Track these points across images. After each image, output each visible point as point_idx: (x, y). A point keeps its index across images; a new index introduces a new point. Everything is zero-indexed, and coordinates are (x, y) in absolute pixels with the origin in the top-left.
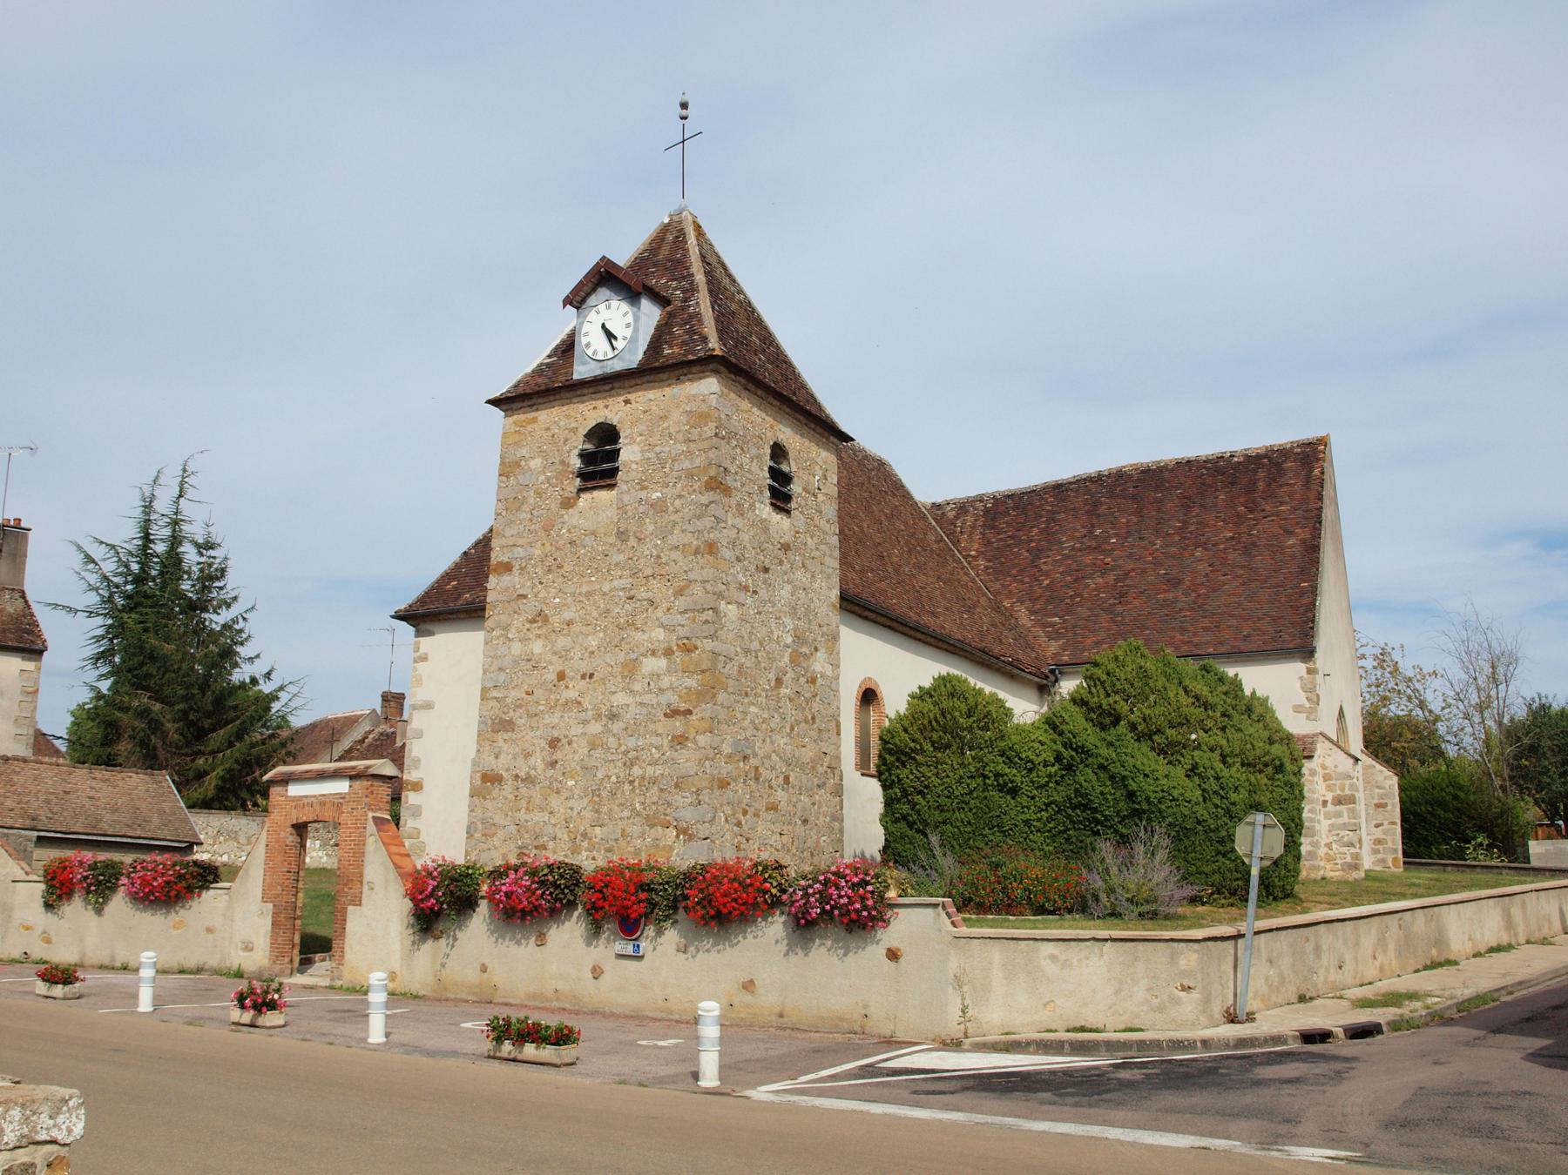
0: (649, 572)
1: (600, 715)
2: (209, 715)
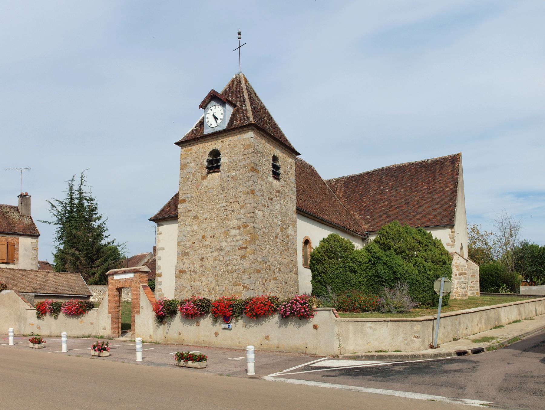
0: (232, 201)
2: (95, 255)
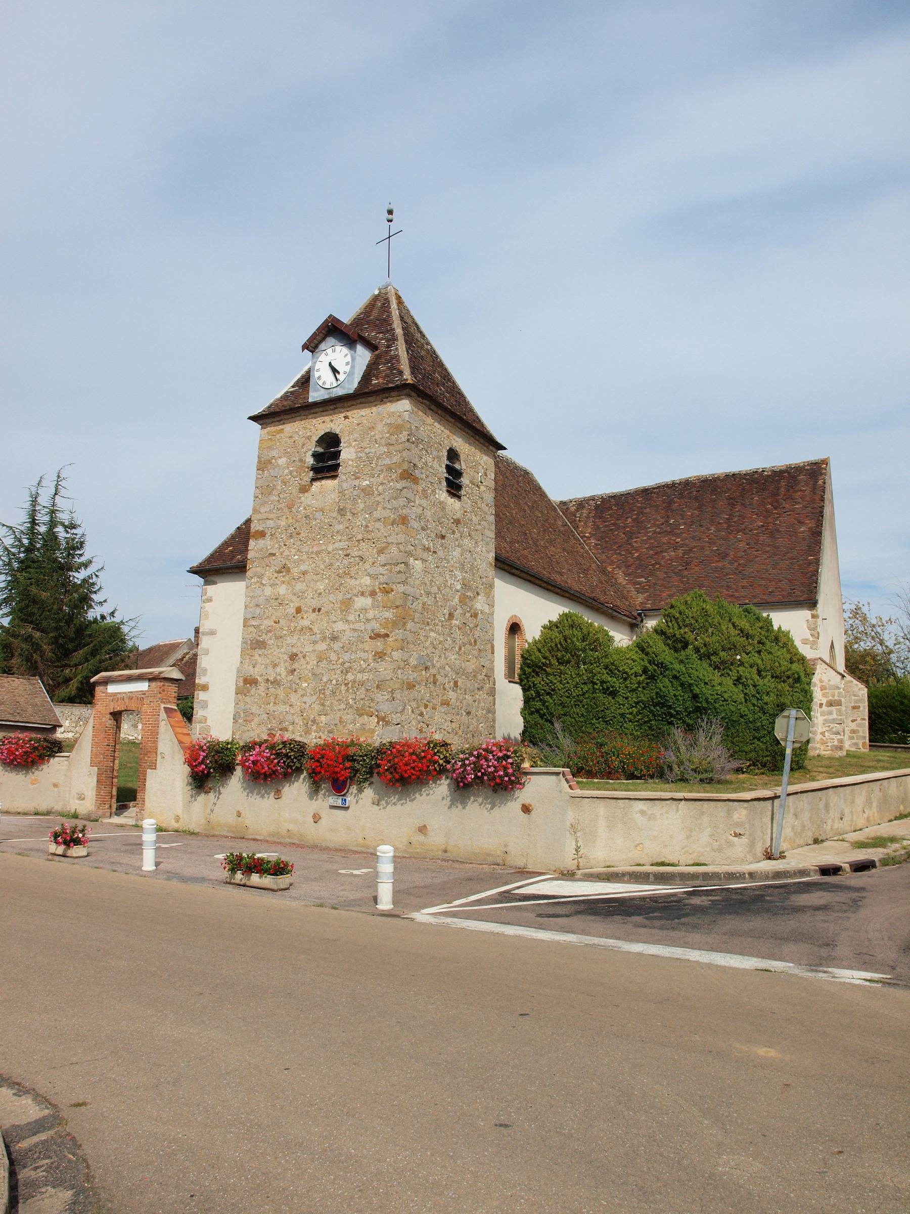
0: (360, 537)
1: (325, 638)
